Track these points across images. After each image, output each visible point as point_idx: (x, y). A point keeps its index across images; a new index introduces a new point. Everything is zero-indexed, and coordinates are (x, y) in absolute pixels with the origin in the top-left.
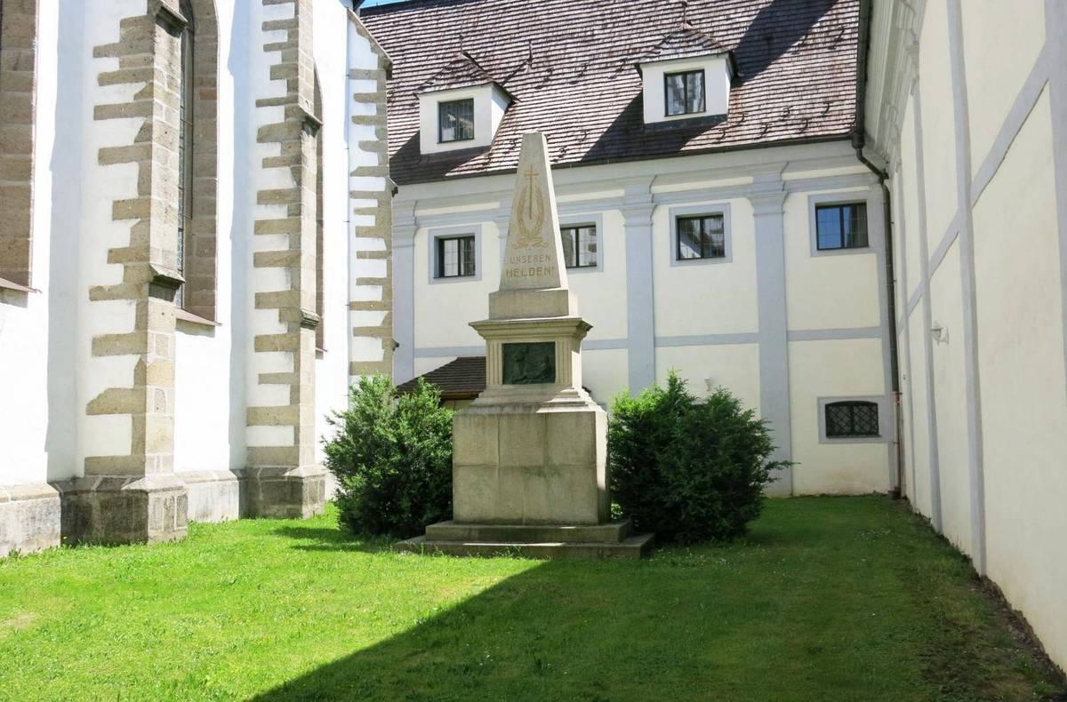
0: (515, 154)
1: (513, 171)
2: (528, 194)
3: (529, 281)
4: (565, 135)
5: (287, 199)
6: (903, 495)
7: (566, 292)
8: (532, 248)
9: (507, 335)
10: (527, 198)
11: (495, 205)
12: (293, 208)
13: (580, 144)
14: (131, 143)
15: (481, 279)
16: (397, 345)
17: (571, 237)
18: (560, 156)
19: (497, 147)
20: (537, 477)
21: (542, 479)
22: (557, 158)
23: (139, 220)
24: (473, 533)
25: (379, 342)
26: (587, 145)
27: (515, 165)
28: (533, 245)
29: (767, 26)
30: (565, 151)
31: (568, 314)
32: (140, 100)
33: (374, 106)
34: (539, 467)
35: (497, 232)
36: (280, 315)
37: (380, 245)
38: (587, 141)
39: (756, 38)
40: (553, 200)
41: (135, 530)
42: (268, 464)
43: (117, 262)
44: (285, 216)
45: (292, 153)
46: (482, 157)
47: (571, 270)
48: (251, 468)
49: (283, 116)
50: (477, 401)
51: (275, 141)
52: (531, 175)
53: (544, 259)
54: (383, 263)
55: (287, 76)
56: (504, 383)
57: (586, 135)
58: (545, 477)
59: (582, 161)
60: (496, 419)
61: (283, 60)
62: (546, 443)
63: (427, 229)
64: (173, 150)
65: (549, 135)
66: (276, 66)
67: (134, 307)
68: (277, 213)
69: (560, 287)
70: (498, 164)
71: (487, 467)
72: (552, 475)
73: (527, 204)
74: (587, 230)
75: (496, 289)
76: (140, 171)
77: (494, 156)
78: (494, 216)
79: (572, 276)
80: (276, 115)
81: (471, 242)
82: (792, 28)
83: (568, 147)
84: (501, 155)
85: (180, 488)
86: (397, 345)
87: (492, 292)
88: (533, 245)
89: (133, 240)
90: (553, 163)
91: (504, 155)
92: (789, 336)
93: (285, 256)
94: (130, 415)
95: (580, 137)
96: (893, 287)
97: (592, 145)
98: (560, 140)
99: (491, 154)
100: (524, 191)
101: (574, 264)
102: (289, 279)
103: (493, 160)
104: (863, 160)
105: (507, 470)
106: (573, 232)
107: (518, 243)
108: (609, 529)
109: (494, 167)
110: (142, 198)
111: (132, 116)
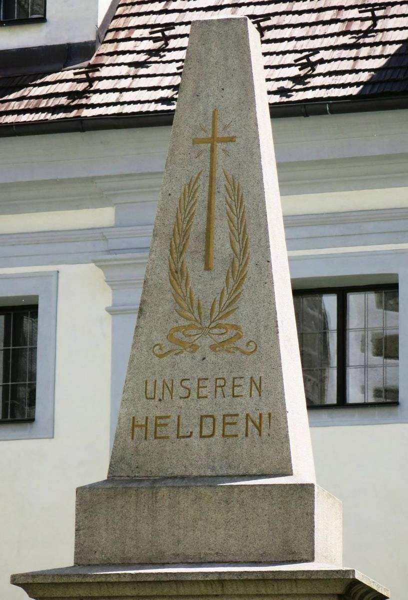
0: (164, 72)
1: (162, 120)
2: (202, 195)
3: (197, 455)
4: (313, 17)
7: (306, 490)
8: (211, 357)
9: (150, 187)
10: (200, 209)
11: (103, 216)
13: (357, 46)
15: (51, 435)
17: (324, 316)
18: (296, 79)
19: (110, 48)
22: (288, 84)
26: (378, 50)
27: (163, 101)
28: (213, 348)
30: (313, 65)
31: (311, 559)
35: (106, 297)
38: (379, 37)
40: (275, 205)
46: (69, 74)
47: (324, 415)
52: (213, 141)
57: (375, 19)
59: (359, 96)
65: (267, 17)
69: (289, 473)
70: (112, 97)
73: (199, 223)
74: (372, 297)
75: (100, 474)
78: (100, 248)
79: (319, 430)
81: (27, 322)
83: (323, 55)
84: (124, 70)
88: (213, 348)
90: (276, 99)
91: (132, 71)
95: (356, 26)
97: (391, 50)
98: (298, 32)
99: (95, 67)
100: (190, 190)
101: (332, 397)
103: (97, 85)
106: (330, 303)
107: (170, 337)
109: (102, 103)
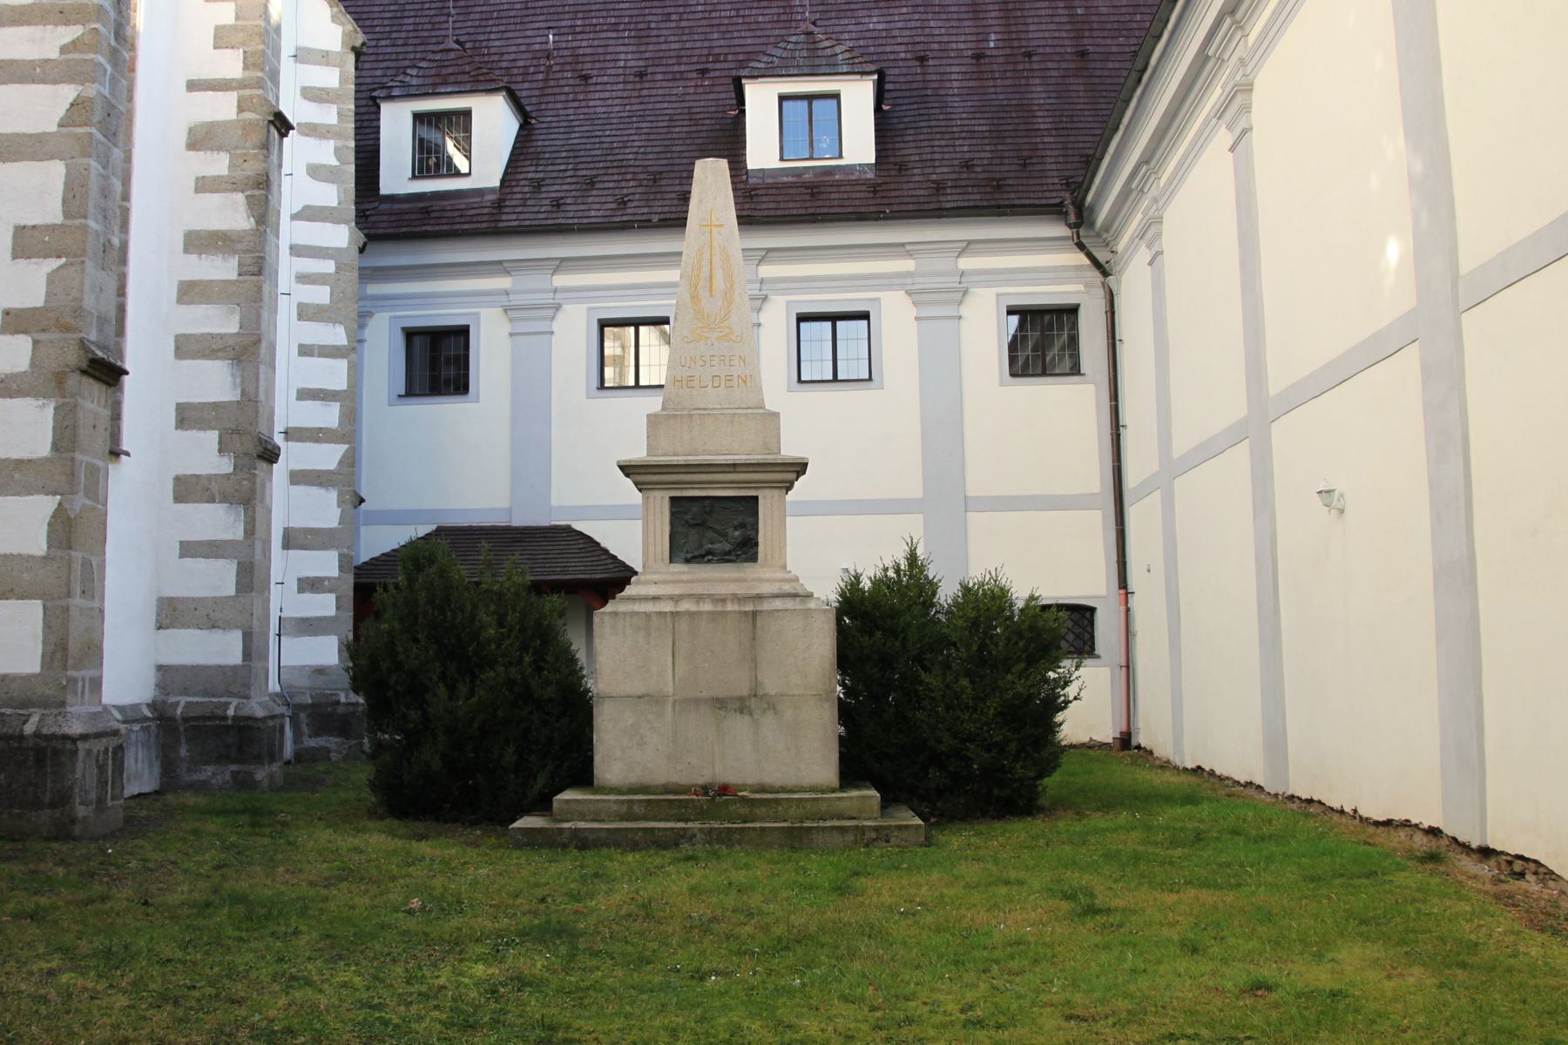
2: (707, 255)
5: (239, 246)
6: (1134, 743)
12: (249, 261)
14: (53, 128)
16: (362, 501)
21: (747, 717)
23: (64, 260)
25: (333, 495)
29: (917, 39)
32: (71, 56)
33: (334, 109)
34: (741, 699)
36: (220, 443)
37: (337, 335)
39: (903, 55)
41: (52, 806)
42: (195, 695)
43: (17, 331)
44: (233, 276)
45: (252, 168)
48: (164, 702)
49: (235, 110)
50: (629, 590)
51: (220, 148)
53: (736, 362)
54: (342, 365)
55: (243, 44)
56: (671, 561)
61: (237, 18)
62: (754, 660)
63: (387, 315)
64: (115, 145)
66: (224, 27)
67: (50, 411)
68: (222, 269)
71: (651, 699)
72: (764, 711)
73: (705, 270)
76: (67, 175)
80: (223, 107)
82: (954, 46)
85: (116, 733)
86: (362, 501)
89: (49, 294)
92: (968, 504)
93: (231, 342)
94: (39, 602)
96: (1118, 436)
102: (238, 380)
104: (1081, 246)
108: (864, 797)
110: (69, 222)
111: (55, 82)
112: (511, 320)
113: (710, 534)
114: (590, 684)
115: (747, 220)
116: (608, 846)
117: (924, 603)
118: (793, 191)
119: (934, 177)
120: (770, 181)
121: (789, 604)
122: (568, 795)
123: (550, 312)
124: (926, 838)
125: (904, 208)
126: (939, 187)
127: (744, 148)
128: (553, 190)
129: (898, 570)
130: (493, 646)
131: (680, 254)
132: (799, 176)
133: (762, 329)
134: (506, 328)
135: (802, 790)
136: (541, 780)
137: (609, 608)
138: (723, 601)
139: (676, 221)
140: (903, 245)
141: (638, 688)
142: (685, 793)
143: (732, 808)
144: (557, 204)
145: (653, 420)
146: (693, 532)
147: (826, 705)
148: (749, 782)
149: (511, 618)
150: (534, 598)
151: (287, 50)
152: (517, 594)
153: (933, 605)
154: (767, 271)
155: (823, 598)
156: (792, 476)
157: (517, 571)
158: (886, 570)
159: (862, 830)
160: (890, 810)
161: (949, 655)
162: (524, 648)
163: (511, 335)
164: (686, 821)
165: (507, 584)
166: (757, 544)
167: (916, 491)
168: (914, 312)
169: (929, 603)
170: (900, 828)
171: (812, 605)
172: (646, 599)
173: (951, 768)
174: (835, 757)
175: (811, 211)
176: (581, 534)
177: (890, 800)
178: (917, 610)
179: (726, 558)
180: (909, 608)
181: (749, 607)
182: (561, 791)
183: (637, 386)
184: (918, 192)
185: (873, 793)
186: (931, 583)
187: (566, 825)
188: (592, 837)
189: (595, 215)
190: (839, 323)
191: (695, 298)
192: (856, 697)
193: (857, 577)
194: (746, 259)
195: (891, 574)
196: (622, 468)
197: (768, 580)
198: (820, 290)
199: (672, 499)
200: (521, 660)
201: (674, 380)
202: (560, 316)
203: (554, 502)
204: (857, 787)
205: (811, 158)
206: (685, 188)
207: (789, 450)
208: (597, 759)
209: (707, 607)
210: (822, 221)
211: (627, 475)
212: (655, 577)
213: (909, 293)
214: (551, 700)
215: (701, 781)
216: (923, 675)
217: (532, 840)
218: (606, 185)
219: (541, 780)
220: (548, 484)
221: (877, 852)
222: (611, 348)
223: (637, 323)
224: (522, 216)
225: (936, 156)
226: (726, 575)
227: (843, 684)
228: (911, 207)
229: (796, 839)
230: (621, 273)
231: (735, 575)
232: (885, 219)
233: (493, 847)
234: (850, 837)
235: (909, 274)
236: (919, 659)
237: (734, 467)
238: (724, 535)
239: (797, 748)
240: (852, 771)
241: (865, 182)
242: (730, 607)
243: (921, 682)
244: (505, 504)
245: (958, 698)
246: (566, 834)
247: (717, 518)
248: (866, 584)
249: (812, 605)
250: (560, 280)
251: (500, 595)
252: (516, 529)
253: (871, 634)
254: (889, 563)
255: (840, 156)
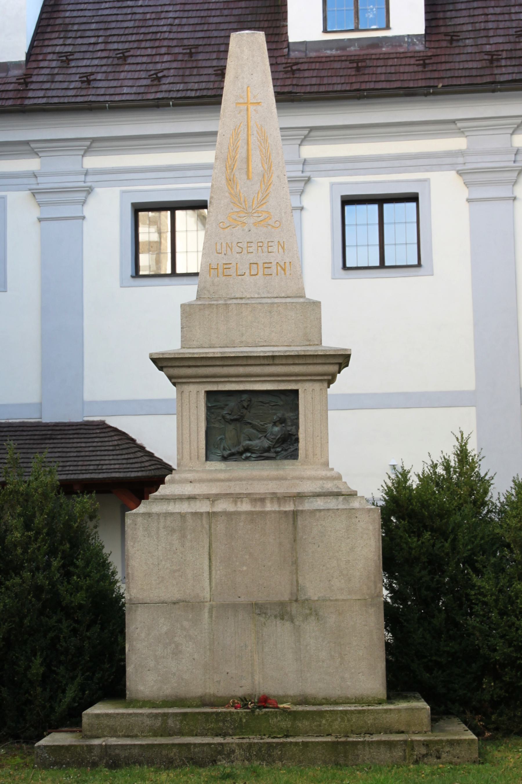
2: (243, 136)
20: (279, 622)
21: (288, 624)
24: (170, 722)
34: (282, 604)
50: (163, 490)
53: (275, 249)
58: (292, 620)
60: (205, 521)
62: (295, 563)
71: (189, 605)
72: (306, 617)
73: (242, 152)
77: (34, 79)
87: (322, 304)
88: (255, 224)
105: (225, 609)
108: (412, 709)
112: (39, 204)
113: (248, 430)
114: (122, 588)
115: (285, 97)
116: (141, 764)
117: (475, 502)
118: (337, 65)
119: (488, 48)
120: (313, 54)
121: (332, 503)
122: (99, 709)
123: (81, 196)
124: (480, 754)
125: (455, 82)
126: (493, 59)
127: (285, 19)
128: (82, 66)
129: (447, 468)
130: (19, 551)
131: (215, 134)
132: (343, 49)
133: (305, 214)
134: (35, 212)
135: (347, 701)
136: (71, 693)
137: (142, 508)
138: (262, 500)
139: (210, 99)
140: (454, 122)
141: (173, 593)
142: (223, 705)
143: (273, 721)
144: (87, 80)
145: (188, 311)
146: (231, 427)
147: (372, 610)
148: (291, 693)
149: (38, 520)
150: (63, 499)
151: (299, 159)
152: (45, 495)
153: (484, 504)
154: (311, 151)
155: (368, 496)
156: (333, 368)
157: (45, 471)
158: (435, 466)
159: (410, 745)
160: (441, 723)
161: (502, 557)
162: (52, 552)
163: (40, 220)
164: (225, 735)
165: (34, 485)
166: (297, 440)
167: (468, 383)
168: (465, 193)
169: (480, 502)
170: (451, 743)
171: (356, 504)
172: (181, 498)
173: (507, 679)
174: (381, 666)
175: (356, 86)
176: (115, 430)
177: (439, 714)
178: (467, 509)
179: (264, 455)
180: (459, 508)
181: (289, 507)
182: (91, 704)
183: (174, 274)
184: (470, 65)
185: (423, 705)
186: (482, 480)
187: (96, 742)
188: (123, 754)
189: (128, 92)
190: (386, 206)
191: (231, 181)
192: (404, 601)
193: (405, 474)
194: (284, 138)
195: (440, 470)
196: (155, 361)
197: (309, 478)
198: (366, 171)
199: (209, 394)
200: (49, 565)
201: (211, 268)
202: (92, 201)
203: (87, 397)
204: (406, 698)
205: (357, 29)
206: (222, 63)
207: (331, 341)
208: (129, 669)
209: (245, 507)
210: (368, 97)
211: (161, 368)
212: (190, 476)
213: (460, 173)
214: (80, 607)
215: (240, 692)
216: (476, 580)
217: (61, 758)
218: (140, 60)
219: (71, 693)
220: (80, 378)
221: (427, 769)
222: (147, 233)
223: (173, 207)
224: (50, 93)
225: (490, 25)
226: (265, 473)
227: (390, 588)
228: (463, 81)
229: (341, 753)
230: (133, 159)
231: (274, 473)
232: (434, 94)
233: (17, 767)
234: (398, 753)
235: (461, 153)
236: (470, 562)
237: (272, 359)
238: (263, 431)
239: (341, 657)
240: (400, 681)
241: (414, 55)
242: (269, 507)
243: (473, 586)
244: (35, 398)
245: (512, 603)
246: (96, 752)
247: (256, 412)
248: (414, 482)
249: (356, 504)
250: (92, 162)
251: (27, 497)
252: (47, 425)
253: (419, 536)
254: (438, 459)
255: (388, 27)
